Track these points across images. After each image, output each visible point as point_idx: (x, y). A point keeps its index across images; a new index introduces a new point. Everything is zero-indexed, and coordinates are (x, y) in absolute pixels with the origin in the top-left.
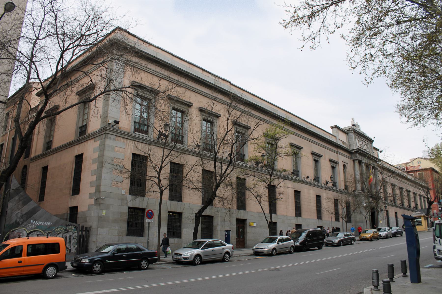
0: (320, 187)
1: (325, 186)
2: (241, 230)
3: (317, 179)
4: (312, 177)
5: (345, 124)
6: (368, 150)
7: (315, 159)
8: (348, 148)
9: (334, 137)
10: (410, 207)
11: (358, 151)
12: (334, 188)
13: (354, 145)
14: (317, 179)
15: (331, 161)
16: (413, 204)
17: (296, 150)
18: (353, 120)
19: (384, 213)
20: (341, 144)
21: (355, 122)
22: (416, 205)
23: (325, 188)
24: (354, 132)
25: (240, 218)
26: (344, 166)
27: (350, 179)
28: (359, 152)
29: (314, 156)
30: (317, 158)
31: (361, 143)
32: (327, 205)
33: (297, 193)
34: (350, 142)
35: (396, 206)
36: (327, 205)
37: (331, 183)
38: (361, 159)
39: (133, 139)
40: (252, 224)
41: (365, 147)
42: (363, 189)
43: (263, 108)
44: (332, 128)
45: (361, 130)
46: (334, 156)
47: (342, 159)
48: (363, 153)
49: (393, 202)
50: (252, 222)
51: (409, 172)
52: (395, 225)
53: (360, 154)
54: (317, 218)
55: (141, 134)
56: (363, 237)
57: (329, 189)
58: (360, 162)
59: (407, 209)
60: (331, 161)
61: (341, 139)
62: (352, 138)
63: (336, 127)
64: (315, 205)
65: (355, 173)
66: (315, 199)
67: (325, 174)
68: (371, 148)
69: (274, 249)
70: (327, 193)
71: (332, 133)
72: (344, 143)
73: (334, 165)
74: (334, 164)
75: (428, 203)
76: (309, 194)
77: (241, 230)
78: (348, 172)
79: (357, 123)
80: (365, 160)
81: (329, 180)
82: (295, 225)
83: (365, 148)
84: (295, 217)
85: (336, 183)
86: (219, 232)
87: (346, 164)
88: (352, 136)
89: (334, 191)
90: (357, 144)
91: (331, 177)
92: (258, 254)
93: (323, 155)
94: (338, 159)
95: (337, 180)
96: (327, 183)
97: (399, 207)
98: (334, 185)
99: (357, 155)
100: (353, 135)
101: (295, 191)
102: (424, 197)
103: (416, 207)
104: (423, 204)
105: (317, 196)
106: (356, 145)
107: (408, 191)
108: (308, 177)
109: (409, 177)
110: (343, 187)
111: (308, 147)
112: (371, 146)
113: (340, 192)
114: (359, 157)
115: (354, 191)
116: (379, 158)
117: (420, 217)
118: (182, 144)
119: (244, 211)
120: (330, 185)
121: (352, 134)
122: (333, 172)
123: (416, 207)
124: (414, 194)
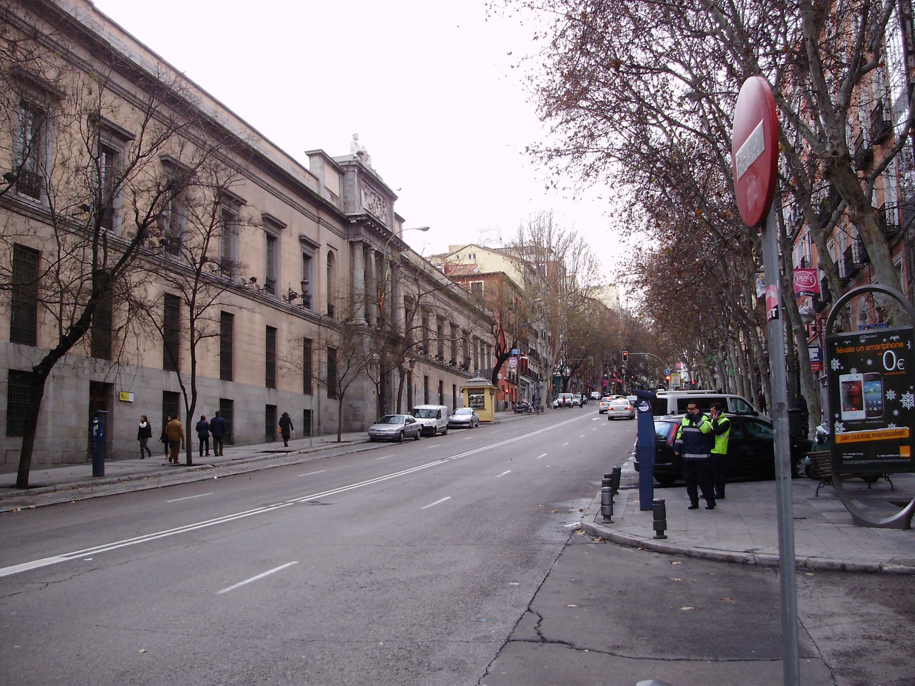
0: (276, 306)
1: (286, 303)
4: (261, 282)
5: (340, 151)
6: (383, 220)
9: (313, 180)
10: (441, 358)
11: (366, 221)
12: (306, 311)
13: (357, 204)
14: (271, 285)
15: (304, 240)
16: (460, 360)
17: (273, 228)
21: (363, 145)
23: (287, 308)
24: (357, 171)
26: (330, 255)
27: (342, 291)
28: (368, 223)
31: (370, 200)
32: (289, 352)
34: (348, 195)
36: (289, 352)
38: (368, 242)
42: (367, 316)
43: (281, 169)
44: (311, 155)
46: (309, 229)
47: (328, 237)
51: (452, 278)
53: (369, 229)
56: (378, 433)
57: (296, 311)
58: (366, 248)
59: (447, 369)
60: (304, 240)
61: (329, 185)
63: (321, 155)
64: (263, 351)
65: (352, 275)
68: (391, 216)
69: (403, 431)
70: (291, 323)
71: (308, 167)
72: (333, 195)
73: (273, 230)
78: (338, 274)
79: (363, 147)
80: (376, 246)
81: (298, 289)
82: (217, 402)
83: (377, 214)
86: (50, 417)
87: (334, 252)
88: (353, 180)
89: (306, 317)
90: (363, 203)
92: (376, 439)
94: (319, 239)
96: (292, 296)
97: (434, 364)
102: (489, 346)
107: (454, 326)
108: (254, 280)
109: (456, 290)
110: (324, 310)
113: (317, 320)
114: (365, 236)
115: (347, 320)
116: (404, 240)
117: (483, 389)
120: (298, 301)
124: (465, 332)
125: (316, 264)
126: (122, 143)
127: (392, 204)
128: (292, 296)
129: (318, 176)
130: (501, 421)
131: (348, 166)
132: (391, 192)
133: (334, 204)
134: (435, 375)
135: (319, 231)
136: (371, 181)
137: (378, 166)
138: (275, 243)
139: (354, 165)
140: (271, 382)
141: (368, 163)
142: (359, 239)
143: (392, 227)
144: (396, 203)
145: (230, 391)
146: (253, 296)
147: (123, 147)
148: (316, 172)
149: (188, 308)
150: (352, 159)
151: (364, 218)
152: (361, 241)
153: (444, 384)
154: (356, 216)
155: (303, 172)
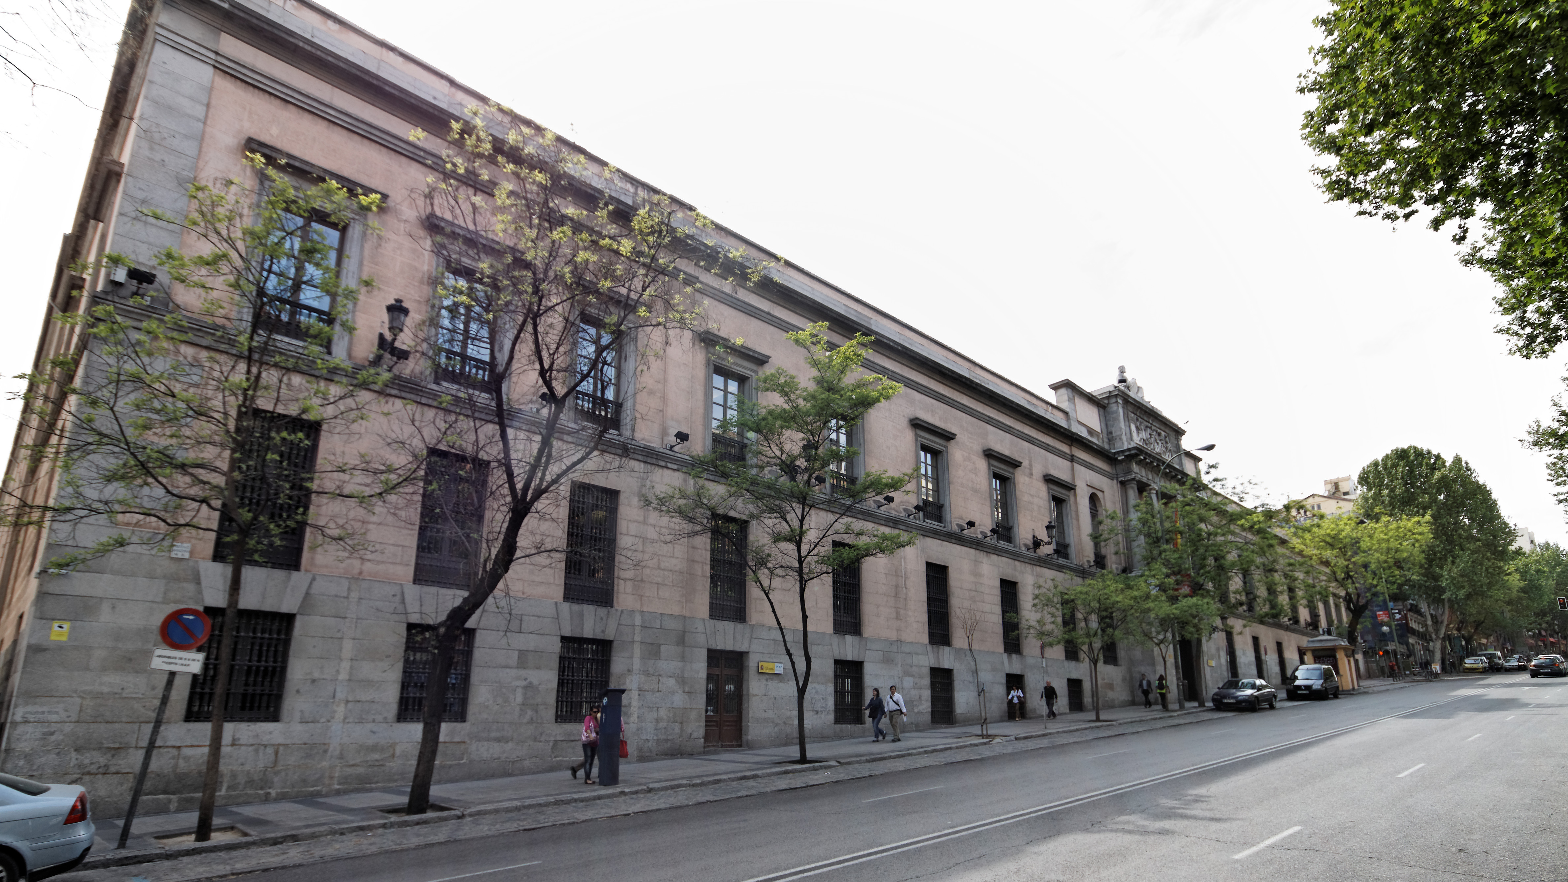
0: (1015, 556)
2: (730, 687)
3: (1004, 531)
5: (1098, 381)
7: (997, 470)
8: (1106, 447)
11: (1136, 455)
13: (1124, 438)
14: (1004, 531)
15: (1049, 480)
18: (1122, 370)
19: (1220, 638)
20: (1084, 433)
22: (1315, 616)
23: (1031, 559)
24: (1123, 401)
25: (720, 646)
28: (1137, 455)
29: (1052, 486)
30: (1060, 492)
31: (1144, 435)
33: (937, 575)
34: (1113, 430)
35: (1279, 626)
37: (1049, 543)
38: (1144, 480)
39: (645, 459)
40: (767, 667)
41: (1158, 449)
44: (1055, 387)
45: (1147, 399)
47: (1086, 478)
48: (1153, 463)
49: (1245, 607)
50: (767, 660)
52: (1255, 672)
54: (1006, 651)
55: (294, 342)
58: (1142, 488)
61: (1087, 419)
62: (1116, 419)
63: (1068, 385)
66: (998, 592)
67: (1032, 519)
70: (1038, 576)
71: (1055, 403)
72: (1091, 431)
73: (1060, 492)
74: (1060, 492)
75: (1348, 608)
76: (975, 580)
77: (730, 687)
80: (1158, 484)
81: (1043, 535)
84: (929, 647)
85: (1066, 546)
87: (1099, 494)
88: (1117, 412)
89: (1060, 568)
90: (1132, 436)
91: (1048, 527)
93: (1025, 463)
95: (1072, 539)
98: (1062, 550)
99: (1135, 467)
100: (1121, 411)
101: (929, 565)
103: (1314, 624)
104: (1333, 610)
105: (1003, 582)
106: (1132, 439)
111: (972, 438)
112: (1178, 447)
113: (1082, 573)
114: (1138, 471)
118: (941, 522)
119: (740, 626)
121: (1119, 410)
122: (1060, 514)
123: (1314, 624)
125: (1073, 508)
126: (1011, 470)
127: (1178, 440)
128: (1037, 543)
129: (1067, 410)
130: (1370, 690)
131: (1108, 398)
132: (1176, 426)
133: (1094, 440)
134: (1268, 636)
135: (1073, 470)
136: (1147, 415)
137: (1154, 397)
138: (1064, 505)
139: (1116, 396)
140: (1012, 643)
141: (1140, 395)
142: (1130, 477)
143: (1181, 464)
144: (1183, 438)
145: (946, 659)
146: (976, 544)
147: (756, 372)
148: (1065, 405)
149: (411, 491)
150: (1112, 389)
151: (1133, 452)
152: (1134, 479)
153: (1285, 645)
154: (1123, 451)
155: (1044, 405)
